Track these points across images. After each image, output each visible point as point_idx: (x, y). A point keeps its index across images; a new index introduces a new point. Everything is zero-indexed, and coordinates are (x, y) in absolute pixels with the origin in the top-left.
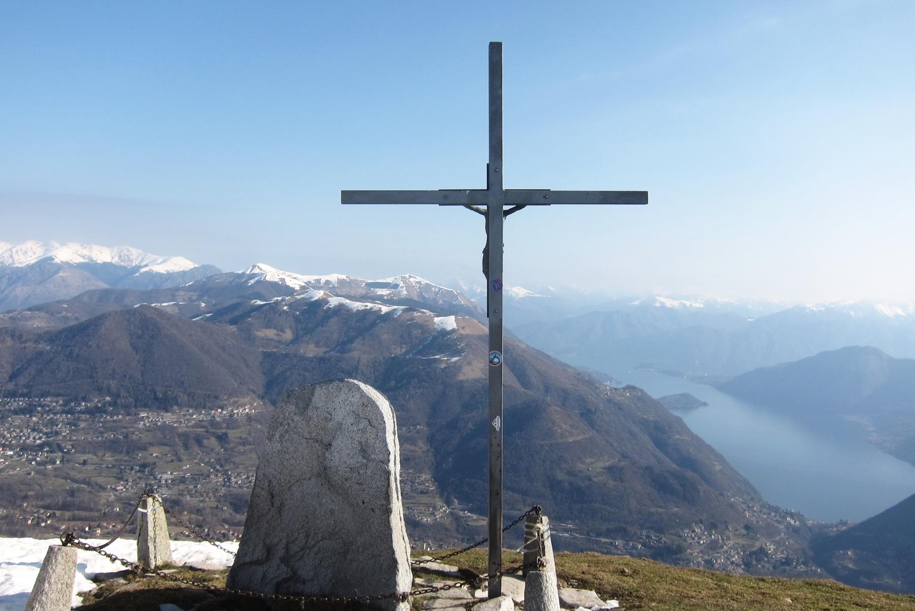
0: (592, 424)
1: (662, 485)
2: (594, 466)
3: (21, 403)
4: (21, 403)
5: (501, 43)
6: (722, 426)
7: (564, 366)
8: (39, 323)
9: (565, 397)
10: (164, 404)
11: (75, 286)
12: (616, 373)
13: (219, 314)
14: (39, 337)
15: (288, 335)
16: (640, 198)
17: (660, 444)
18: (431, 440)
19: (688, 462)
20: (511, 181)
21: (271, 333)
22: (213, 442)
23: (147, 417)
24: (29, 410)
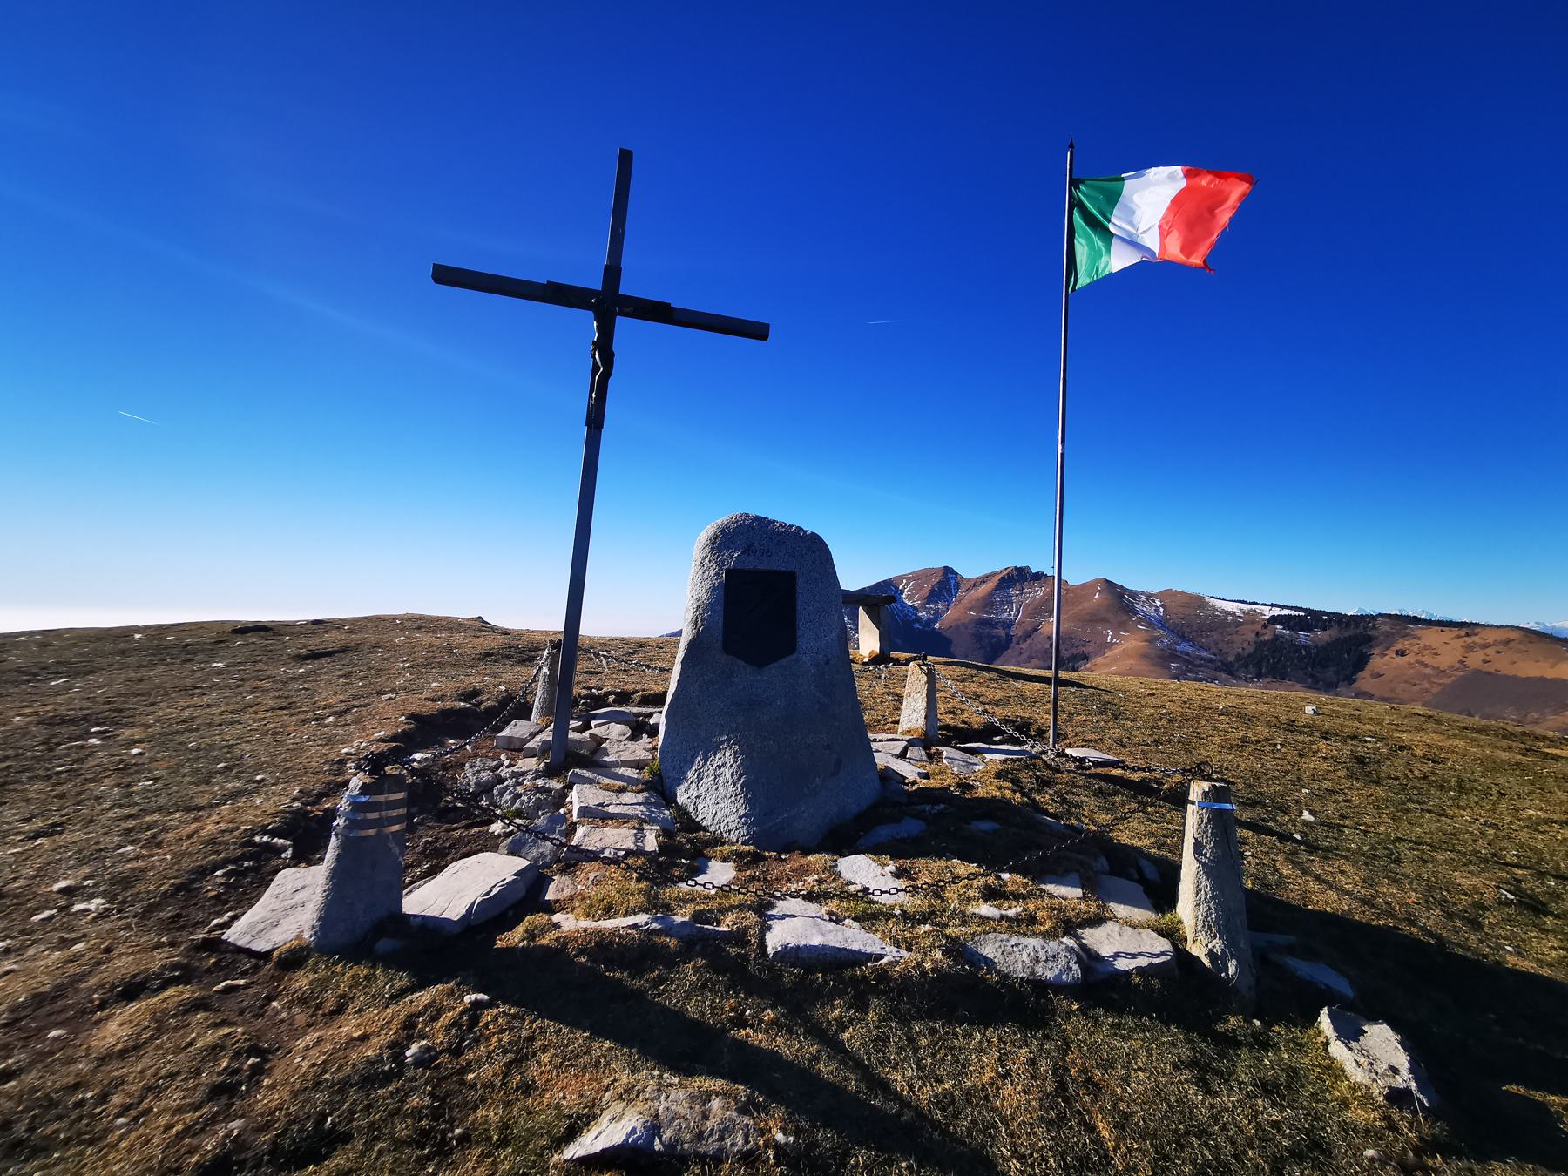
5: (791, 577)
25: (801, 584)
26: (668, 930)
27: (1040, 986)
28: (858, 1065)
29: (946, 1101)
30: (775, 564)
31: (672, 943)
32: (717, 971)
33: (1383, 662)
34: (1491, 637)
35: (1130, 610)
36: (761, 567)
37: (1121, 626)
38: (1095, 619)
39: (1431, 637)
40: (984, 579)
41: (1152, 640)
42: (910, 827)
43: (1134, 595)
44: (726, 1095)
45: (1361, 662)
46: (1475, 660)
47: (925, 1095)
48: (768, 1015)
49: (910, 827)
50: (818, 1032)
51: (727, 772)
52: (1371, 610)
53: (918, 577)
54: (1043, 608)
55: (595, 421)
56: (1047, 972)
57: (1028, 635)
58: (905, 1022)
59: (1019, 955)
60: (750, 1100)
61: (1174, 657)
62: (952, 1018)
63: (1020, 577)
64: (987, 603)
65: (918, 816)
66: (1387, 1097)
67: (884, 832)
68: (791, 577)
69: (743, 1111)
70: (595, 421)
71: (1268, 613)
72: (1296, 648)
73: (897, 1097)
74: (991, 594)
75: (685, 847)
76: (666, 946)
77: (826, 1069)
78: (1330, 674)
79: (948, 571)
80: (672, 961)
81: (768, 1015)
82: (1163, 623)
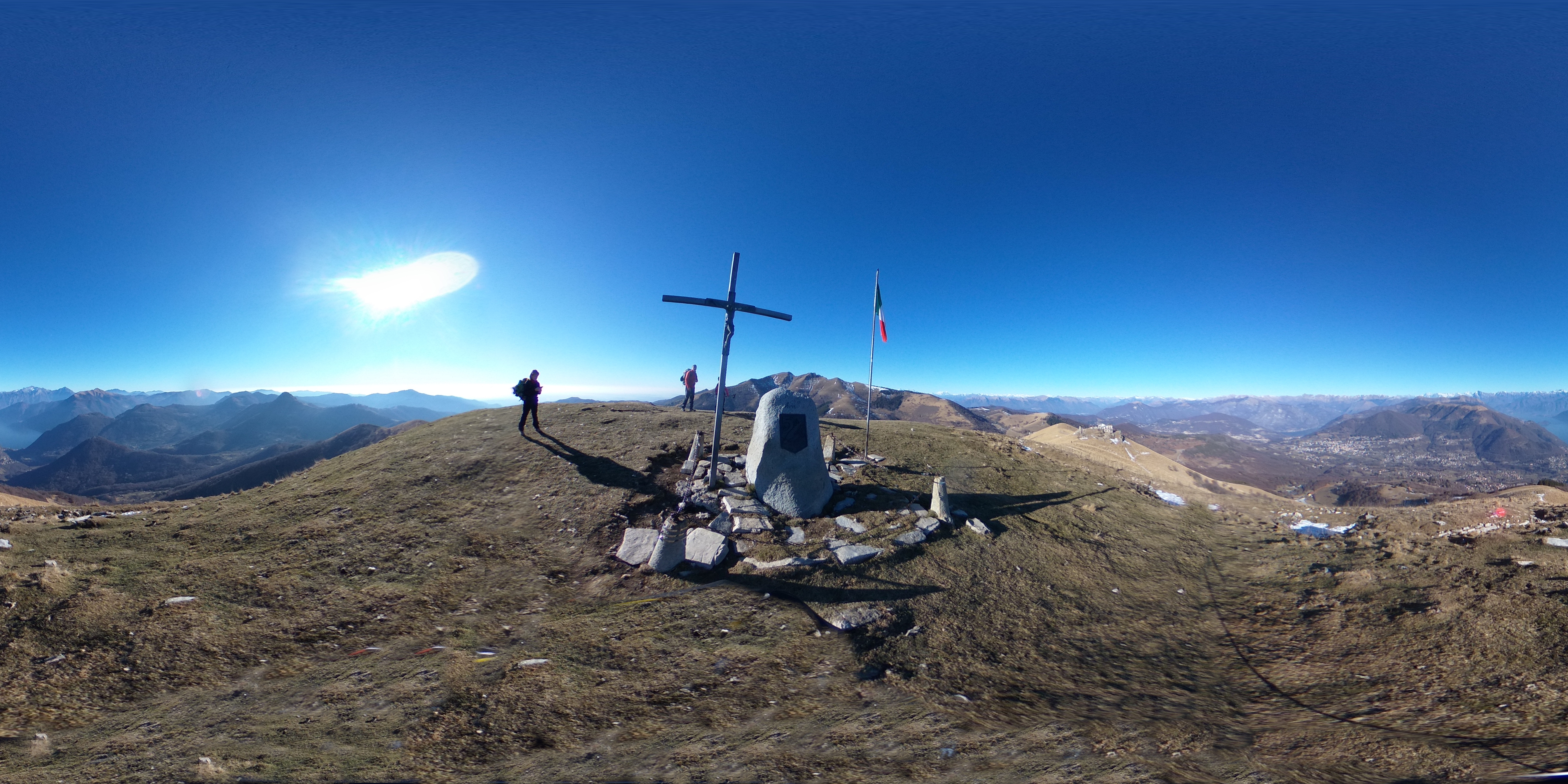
0: (1520, 432)
1: (1541, 446)
2: (1522, 445)
3: (1358, 438)
4: (1358, 438)
5: (804, 416)
6: (1511, 414)
7: (1510, 417)
8: (1360, 417)
9: (1511, 426)
10: (1395, 437)
11: (1368, 406)
12: (1523, 417)
13: (1409, 411)
14: (1362, 420)
15: (1429, 415)
16: (788, 318)
17: (1539, 436)
18: (1473, 442)
19: (1549, 440)
20: (737, 300)
21: (1424, 415)
22: (1410, 447)
23: (1391, 441)
24: (1360, 440)
25: (807, 419)
26: (804, 563)
27: (918, 543)
28: (888, 582)
29: (918, 581)
30: (798, 411)
31: (807, 567)
32: (827, 573)
33: (905, 403)
34: (925, 396)
35: (845, 388)
36: (793, 413)
37: (842, 393)
38: (835, 390)
39: (915, 396)
40: (801, 377)
41: (850, 397)
42: (849, 501)
43: (846, 383)
44: (862, 606)
45: (901, 402)
46: (922, 402)
47: (912, 582)
48: (854, 581)
49: (849, 501)
50: (871, 579)
51: (787, 493)
52: (903, 389)
53: (780, 375)
54: (820, 386)
55: (726, 352)
56: (918, 539)
57: (814, 395)
58: (893, 567)
59: (910, 537)
60: (871, 605)
61: (856, 402)
62: (904, 561)
63: (812, 376)
64: (802, 384)
65: (850, 496)
66: (922, 548)
67: (841, 505)
68: (804, 416)
69: (870, 608)
70: (726, 352)
71: (880, 389)
72: (886, 399)
73: (905, 585)
74: (803, 382)
75: (780, 527)
76: (805, 569)
77: (882, 587)
78: (893, 406)
79: (789, 373)
80: (810, 573)
81: (854, 581)
82: (853, 392)
